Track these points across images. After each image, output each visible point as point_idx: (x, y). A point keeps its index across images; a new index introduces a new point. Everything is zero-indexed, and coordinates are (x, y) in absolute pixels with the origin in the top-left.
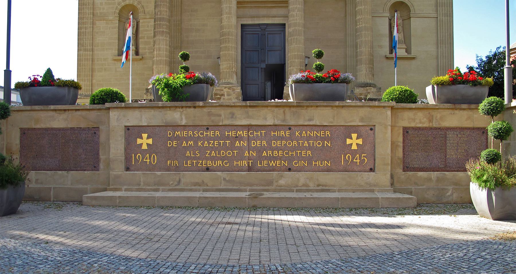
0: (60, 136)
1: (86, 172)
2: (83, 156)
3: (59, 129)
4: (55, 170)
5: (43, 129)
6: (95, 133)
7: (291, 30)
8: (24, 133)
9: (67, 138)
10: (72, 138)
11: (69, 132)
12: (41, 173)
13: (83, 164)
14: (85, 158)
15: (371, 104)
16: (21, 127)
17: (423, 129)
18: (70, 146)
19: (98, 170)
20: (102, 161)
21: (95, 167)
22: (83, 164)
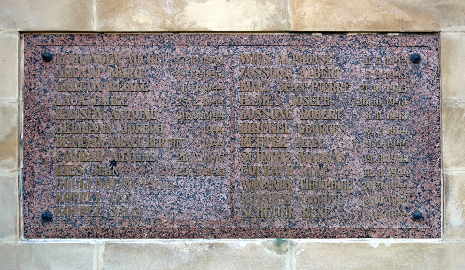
0: (237, 73)
1: (374, 242)
2: (358, 167)
3: (231, 39)
4: (211, 233)
5: (147, 34)
6: (416, 60)
7: (292, 24)
8: (47, 58)
9: (272, 82)
10: (296, 82)
11: (284, 52)
12: (139, 248)
13: (355, 204)
14: (369, 176)
15: (21, 220)
16: (33, 25)
17: (121, 235)
18: (289, 118)
19: (434, 232)
20: (455, 192)
21: (417, 218)
22: (355, 204)
